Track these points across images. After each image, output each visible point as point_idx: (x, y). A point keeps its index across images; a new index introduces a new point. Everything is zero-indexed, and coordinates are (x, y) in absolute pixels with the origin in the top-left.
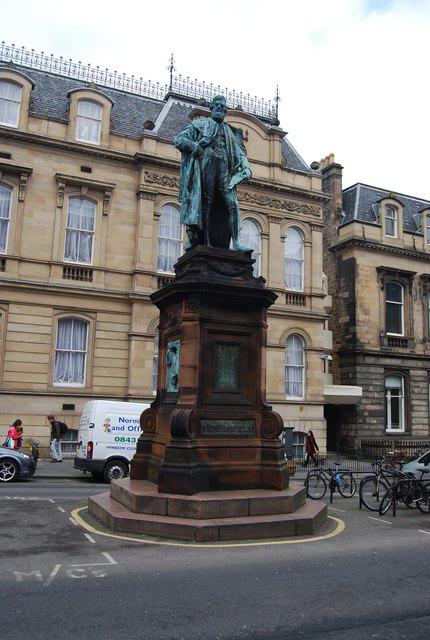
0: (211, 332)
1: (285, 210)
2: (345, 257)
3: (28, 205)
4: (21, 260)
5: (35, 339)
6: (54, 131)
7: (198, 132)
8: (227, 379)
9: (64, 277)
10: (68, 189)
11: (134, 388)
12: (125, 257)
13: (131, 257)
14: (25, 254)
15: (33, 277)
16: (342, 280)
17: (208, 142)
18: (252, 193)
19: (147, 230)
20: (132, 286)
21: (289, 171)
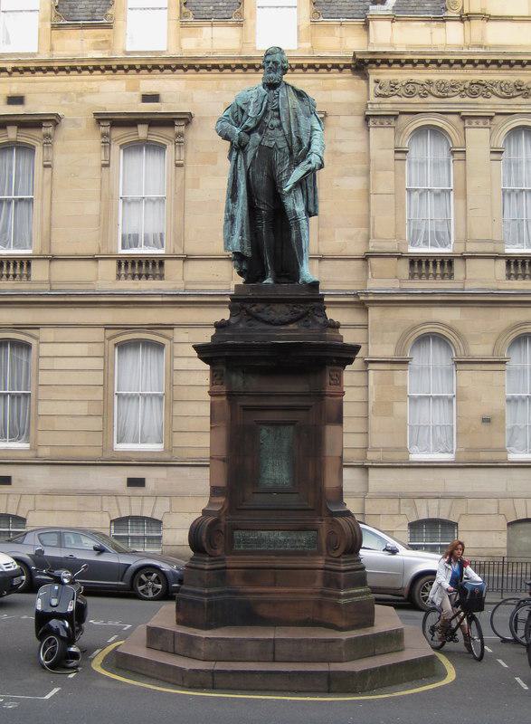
0: (246, 409)
3: (190, 171)
7: (243, 111)
8: (276, 473)
11: (376, 450)
12: (353, 231)
13: (364, 230)
14: (191, 248)
17: (252, 125)
19: (383, 182)
20: (365, 282)
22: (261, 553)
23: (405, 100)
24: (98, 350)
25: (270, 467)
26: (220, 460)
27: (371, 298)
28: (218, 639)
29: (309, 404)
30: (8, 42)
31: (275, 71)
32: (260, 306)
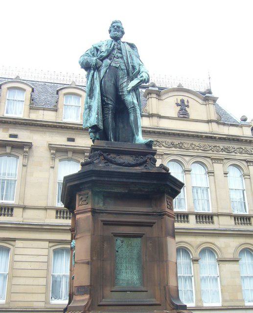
0: (106, 223)
1: (224, 153)
4: (24, 208)
5: (34, 266)
6: (48, 116)
8: (129, 275)
9: (57, 217)
10: (58, 154)
15: (33, 219)
18: (197, 143)
21: (224, 124)
24: (45, 252)
25: (124, 271)
26: (83, 263)
29: (154, 221)
30: (7, 113)
31: (118, 32)
32: (112, 155)
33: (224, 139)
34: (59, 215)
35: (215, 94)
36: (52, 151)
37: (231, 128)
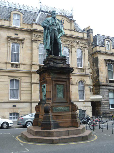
0: (55, 81)
1: (76, 44)
2: (95, 57)
5: (4, 86)
7: (48, 22)
9: (11, 67)
11: (33, 99)
16: (94, 64)
21: (77, 32)
22: (58, 112)
23: (38, 38)
25: (59, 94)
27: (33, 72)
28: (57, 131)
32: (55, 60)
33: (77, 38)
34: (12, 66)
35: (74, 18)
36: (9, 39)
37: (80, 33)
